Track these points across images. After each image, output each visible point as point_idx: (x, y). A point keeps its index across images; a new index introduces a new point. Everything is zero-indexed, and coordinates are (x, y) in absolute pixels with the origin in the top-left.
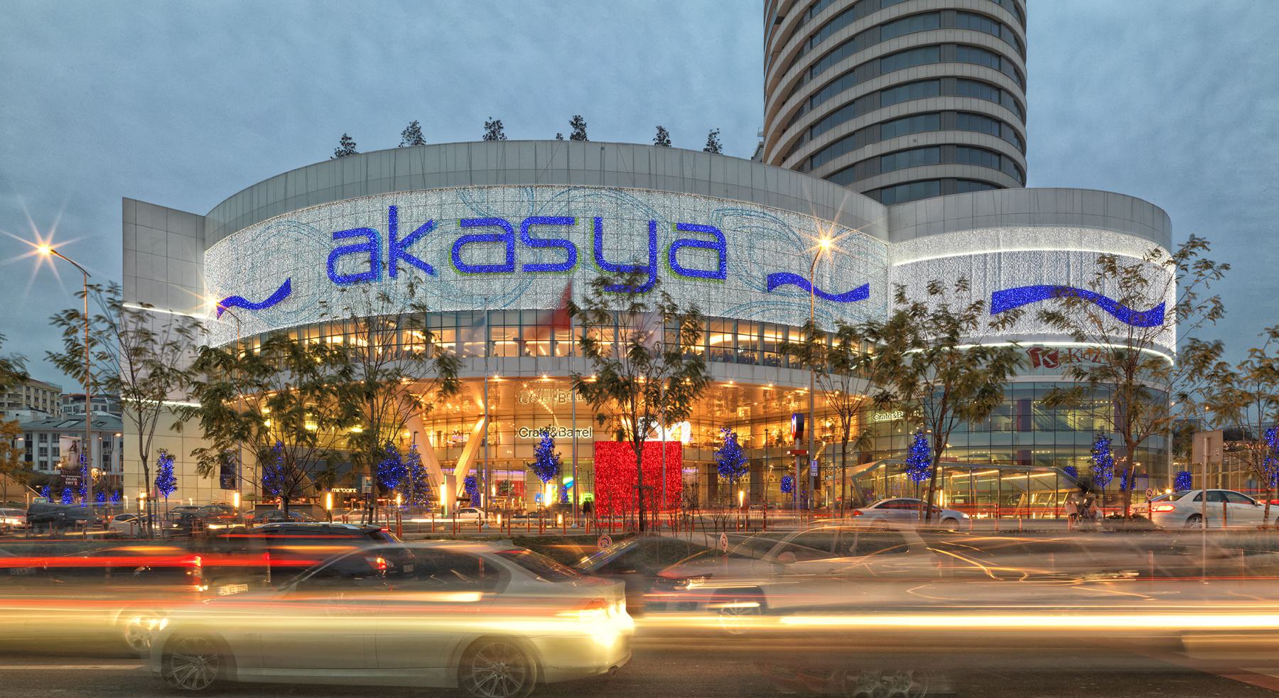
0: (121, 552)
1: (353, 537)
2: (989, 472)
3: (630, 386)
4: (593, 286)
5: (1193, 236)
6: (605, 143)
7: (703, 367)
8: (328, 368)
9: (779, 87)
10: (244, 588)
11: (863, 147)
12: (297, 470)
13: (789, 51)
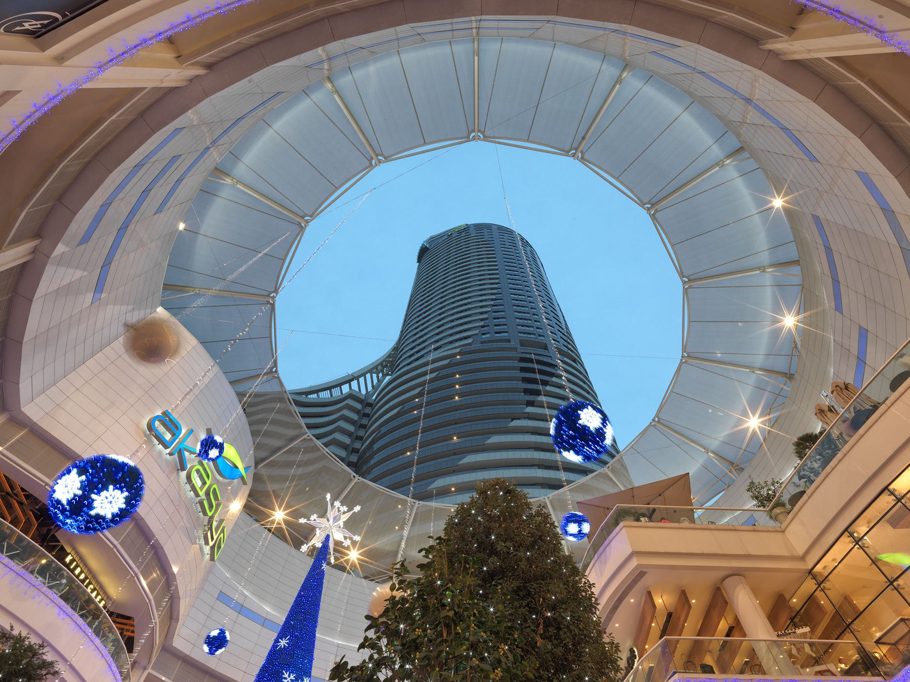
0: (560, 151)
1: (325, 395)
2: (228, 45)
3: (279, 679)
4: (220, 443)
5: (108, 491)
6: (386, 162)
7: (210, 636)
8: (584, 659)
9: (605, 174)
10: (646, 677)
11: (188, 656)
12: (208, 135)
13: (417, 382)
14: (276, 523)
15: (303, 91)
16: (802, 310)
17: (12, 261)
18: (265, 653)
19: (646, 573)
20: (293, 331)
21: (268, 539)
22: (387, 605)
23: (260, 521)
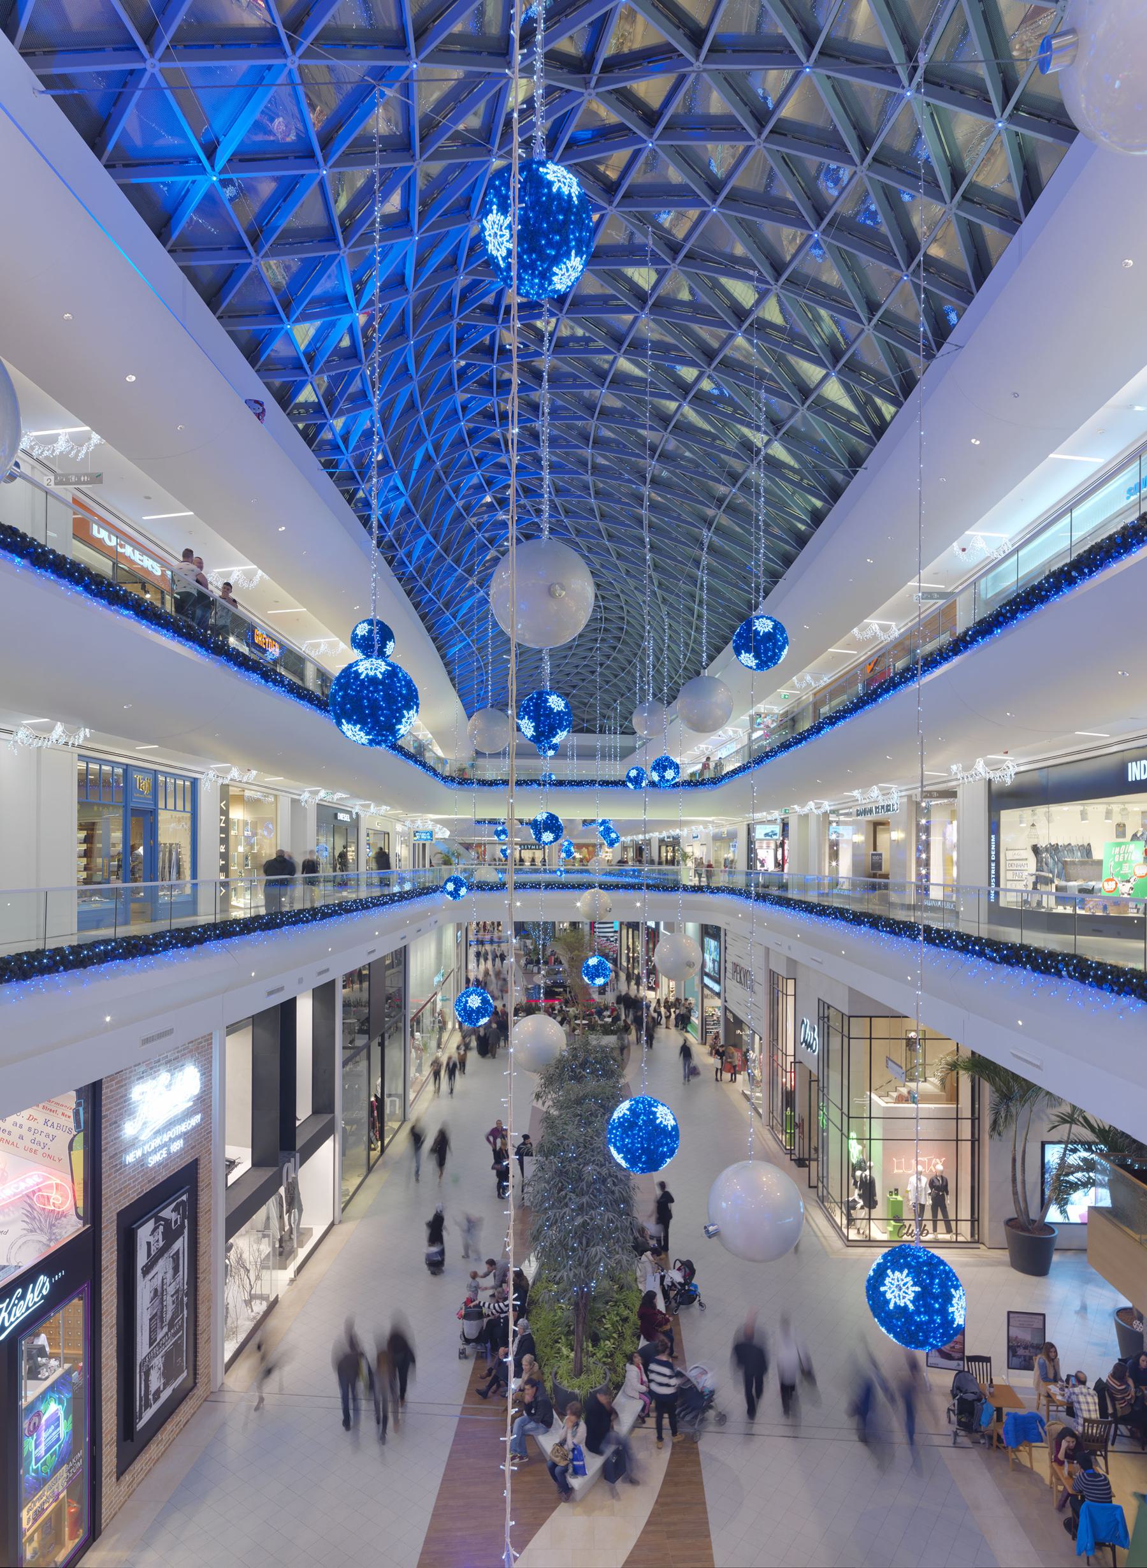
14: (299, 868)
15: (767, 950)
16: (667, 1433)
17: (1124, 1231)
18: (530, 1546)
19: (197, 1160)
20: (888, 1059)
21: (168, 93)
22: (490, 1370)
23: (348, 1068)
